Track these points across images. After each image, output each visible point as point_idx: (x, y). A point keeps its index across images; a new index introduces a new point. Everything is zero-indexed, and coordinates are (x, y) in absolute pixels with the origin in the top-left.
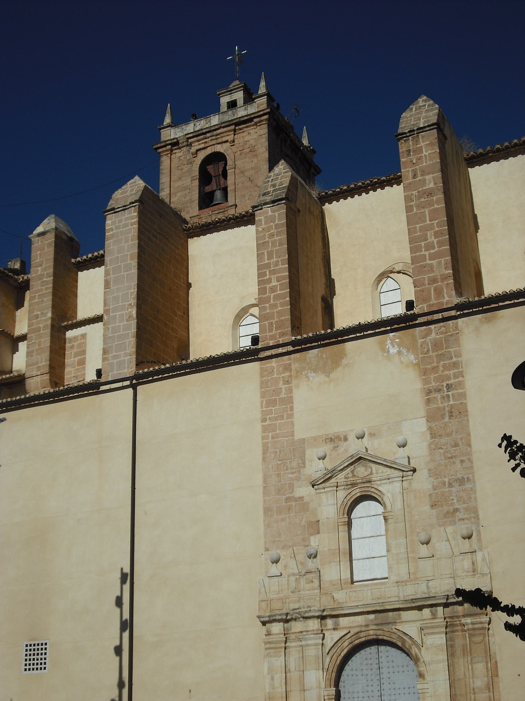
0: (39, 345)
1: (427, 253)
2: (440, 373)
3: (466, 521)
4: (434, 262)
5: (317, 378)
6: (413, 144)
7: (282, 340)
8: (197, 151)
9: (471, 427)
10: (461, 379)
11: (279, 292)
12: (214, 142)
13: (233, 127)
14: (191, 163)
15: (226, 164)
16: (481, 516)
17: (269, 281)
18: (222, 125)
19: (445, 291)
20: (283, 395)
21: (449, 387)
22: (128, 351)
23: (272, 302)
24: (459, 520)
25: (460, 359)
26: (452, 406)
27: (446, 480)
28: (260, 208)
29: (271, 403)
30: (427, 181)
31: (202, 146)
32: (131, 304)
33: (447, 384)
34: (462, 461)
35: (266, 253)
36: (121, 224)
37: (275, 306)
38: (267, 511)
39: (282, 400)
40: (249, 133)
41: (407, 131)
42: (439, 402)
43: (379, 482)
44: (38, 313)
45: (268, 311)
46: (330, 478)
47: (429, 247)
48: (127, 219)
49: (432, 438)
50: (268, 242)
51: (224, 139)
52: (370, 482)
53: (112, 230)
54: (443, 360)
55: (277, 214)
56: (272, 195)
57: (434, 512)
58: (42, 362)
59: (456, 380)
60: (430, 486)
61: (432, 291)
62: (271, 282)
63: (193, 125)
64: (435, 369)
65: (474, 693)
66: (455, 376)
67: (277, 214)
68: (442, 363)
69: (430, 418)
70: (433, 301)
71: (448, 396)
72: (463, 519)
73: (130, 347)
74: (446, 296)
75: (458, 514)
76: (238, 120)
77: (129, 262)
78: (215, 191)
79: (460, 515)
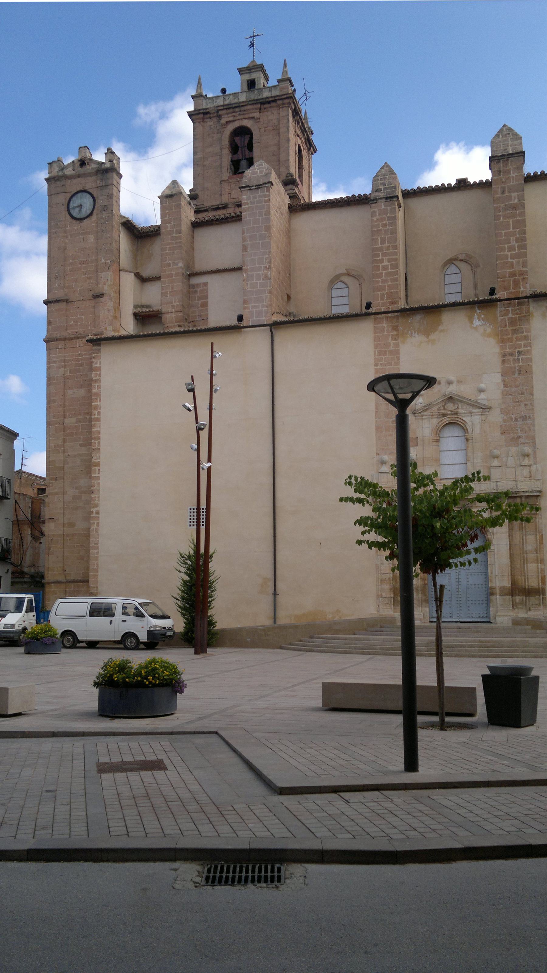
0: (173, 288)
1: (509, 254)
2: (514, 342)
3: (526, 445)
4: (514, 261)
5: (418, 338)
6: (503, 166)
7: (392, 308)
8: (227, 122)
9: (534, 382)
10: (529, 348)
11: (389, 271)
12: (242, 117)
13: (259, 105)
14: (220, 132)
15: (251, 138)
16: (537, 442)
17: (382, 261)
18: (250, 103)
19: (521, 283)
20: (391, 348)
21: (519, 353)
22: (265, 304)
23: (384, 277)
24: (521, 443)
25: (529, 334)
26: (520, 367)
27: (513, 416)
28: (375, 201)
29: (380, 353)
30: (513, 198)
31: (231, 119)
32: (266, 267)
33: (519, 351)
34: (526, 405)
35: (379, 239)
36: (255, 200)
37: (386, 281)
38: (378, 428)
39: (391, 352)
40: (272, 113)
41: (499, 155)
42: (512, 363)
43: (464, 415)
44: (170, 262)
45: (380, 284)
46: (427, 409)
47: (511, 249)
48: (260, 196)
49: (505, 387)
50: (381, 230)
51: (251, 115)
52: (457, 414)
53: (247, 204)
54: (516, 333)
55: (389, 208)
56: (384, 192)
57: (503, 437)
58: (175, 302)
59: (526, 349)
60: (501, 420)
61: (511, 283)
62: (383, 262)
63: (223, 98)
64: (510, 340)
65: (527, 554)
66: (525, 346)
67: (389, 208)
68: (515, 335)
69: (504, 374)
70: (512, 290)
71: (519, 359)
72: (524, 443)
73: (267, 300)
74: (521, 287)
75: (521, 439)
76: (264, 100)
77: (263, 232)
78: (240, 160)
79: (521, 440)
